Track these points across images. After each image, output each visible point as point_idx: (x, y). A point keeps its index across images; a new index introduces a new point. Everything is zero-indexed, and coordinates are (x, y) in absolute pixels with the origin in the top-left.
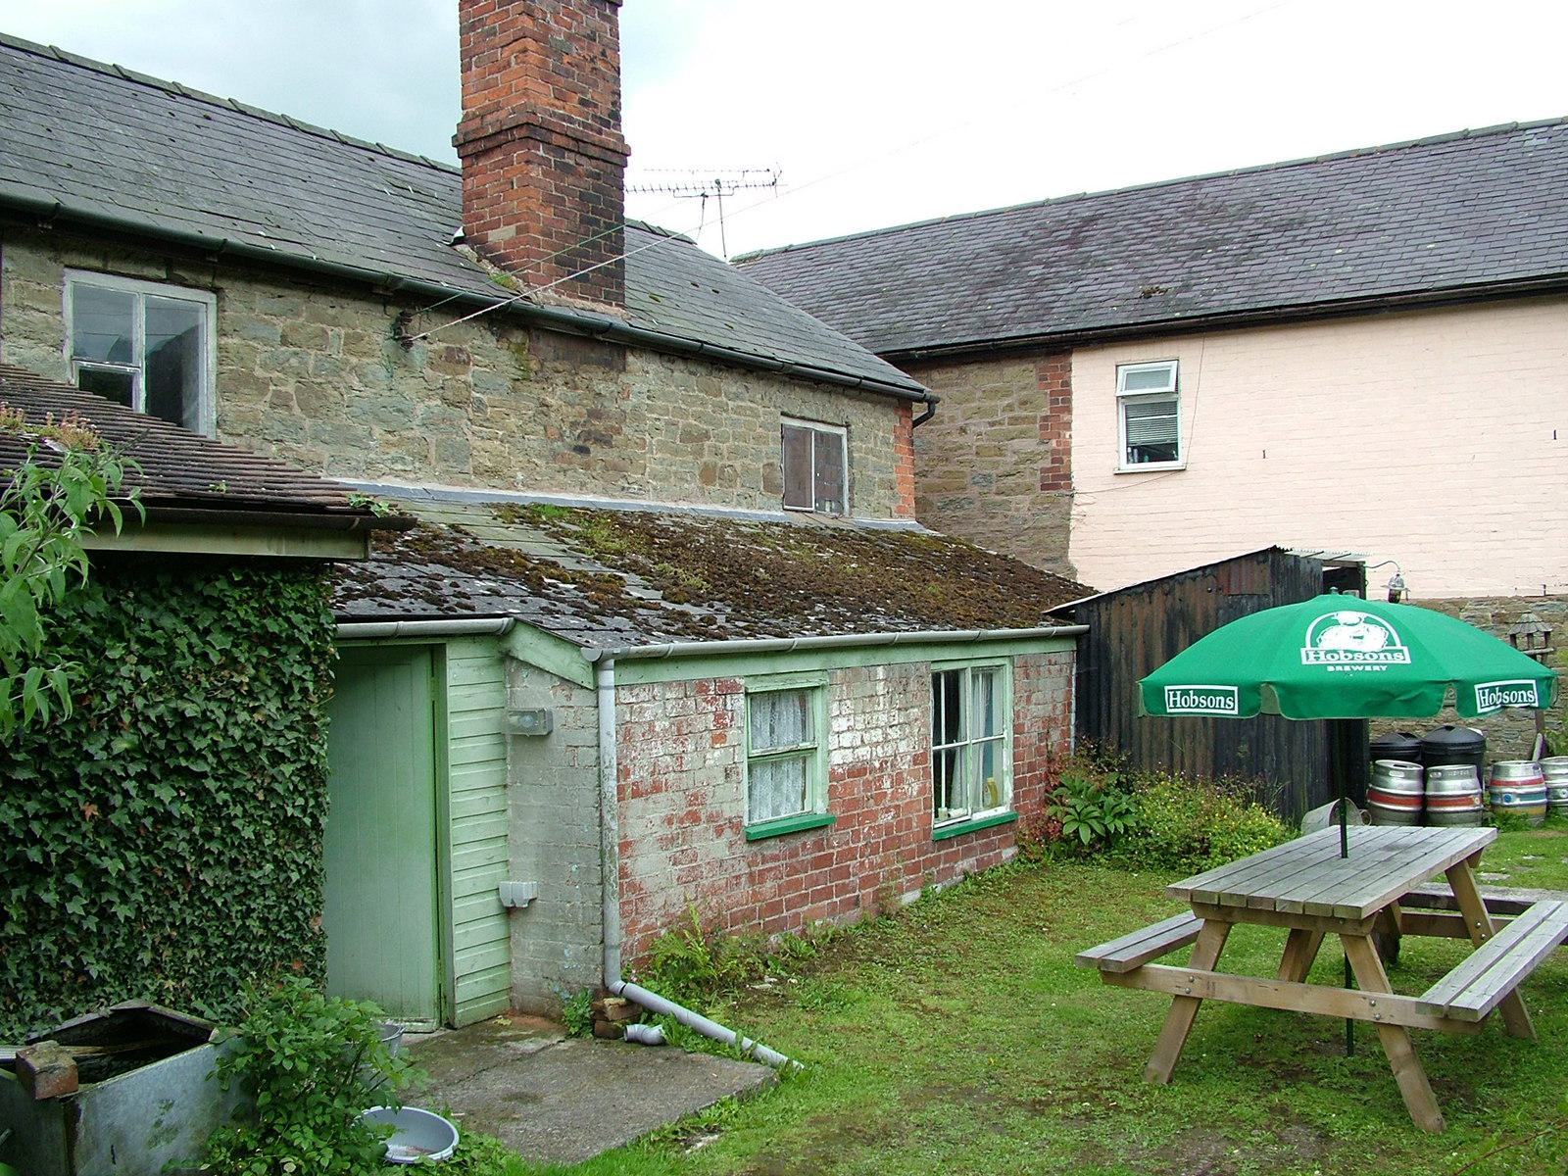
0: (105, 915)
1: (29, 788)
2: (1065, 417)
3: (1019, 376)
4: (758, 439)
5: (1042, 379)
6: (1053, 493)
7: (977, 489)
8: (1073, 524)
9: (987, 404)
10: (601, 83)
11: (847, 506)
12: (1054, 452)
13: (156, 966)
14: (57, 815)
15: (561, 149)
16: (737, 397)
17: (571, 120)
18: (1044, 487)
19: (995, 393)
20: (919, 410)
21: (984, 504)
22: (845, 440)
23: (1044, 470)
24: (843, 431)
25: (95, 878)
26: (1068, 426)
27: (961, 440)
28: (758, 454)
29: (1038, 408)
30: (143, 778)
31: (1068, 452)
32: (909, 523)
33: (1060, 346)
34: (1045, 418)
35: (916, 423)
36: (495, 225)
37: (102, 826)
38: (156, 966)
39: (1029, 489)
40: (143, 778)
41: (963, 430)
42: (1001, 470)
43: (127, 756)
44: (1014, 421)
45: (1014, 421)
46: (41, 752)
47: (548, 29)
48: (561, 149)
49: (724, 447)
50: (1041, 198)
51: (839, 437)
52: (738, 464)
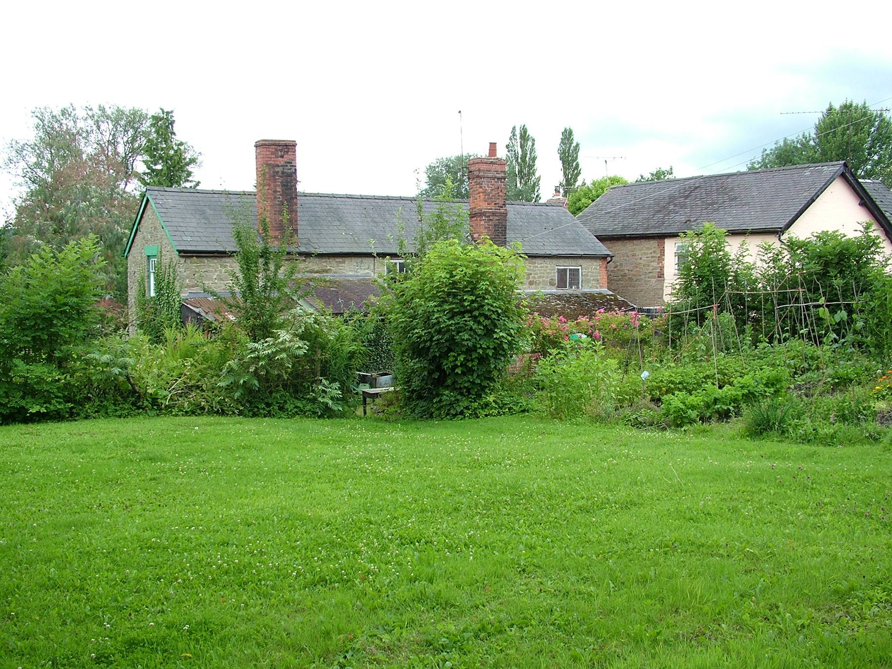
0: (382, 361)
1: (374, 346)
2: (663, 257)
3: (653, 243)
4: (548, 273)
5: (658, 245)
6: (661, 279)
7: (643, 276)
8: (664, 288)
9: (646, 251)
10: (500, 198)
11: (580, 287)
12: (661, 267)
13: (388, 368)
14: (377, 349)
15: (489, 216)
16: (541, 264)
17: (492, 209)
18: (658, 277)
19: (648, 249)
20: (609, 259)
21: (645, 281)
22: (580, 270)
23: (658, 272)
24: (580, 267)
25: (381, 357)
26: (664, 260)
27: (640, 261)
28: (547, 277)
29: (657, 254)
30: (387, 345)
31: (663, 267)
32: (605, 291)
33: (662, 237)
34: (659, 257)
35: (608, 263)
36: (475, 233)
37: (382, 351)
38: (388, 368)
39: (654, 278)
40: (387, 345)
41: (641, 259)
42: (649, 271)
43: (385, 342)
44: (652, 257)
45: (652, 257)
46: (375, 342)
47: (486, 190)
48: (489, 216)
49: (536, 276)
50: (691, 176)
51: (578, 269)
52: (541, 280)
